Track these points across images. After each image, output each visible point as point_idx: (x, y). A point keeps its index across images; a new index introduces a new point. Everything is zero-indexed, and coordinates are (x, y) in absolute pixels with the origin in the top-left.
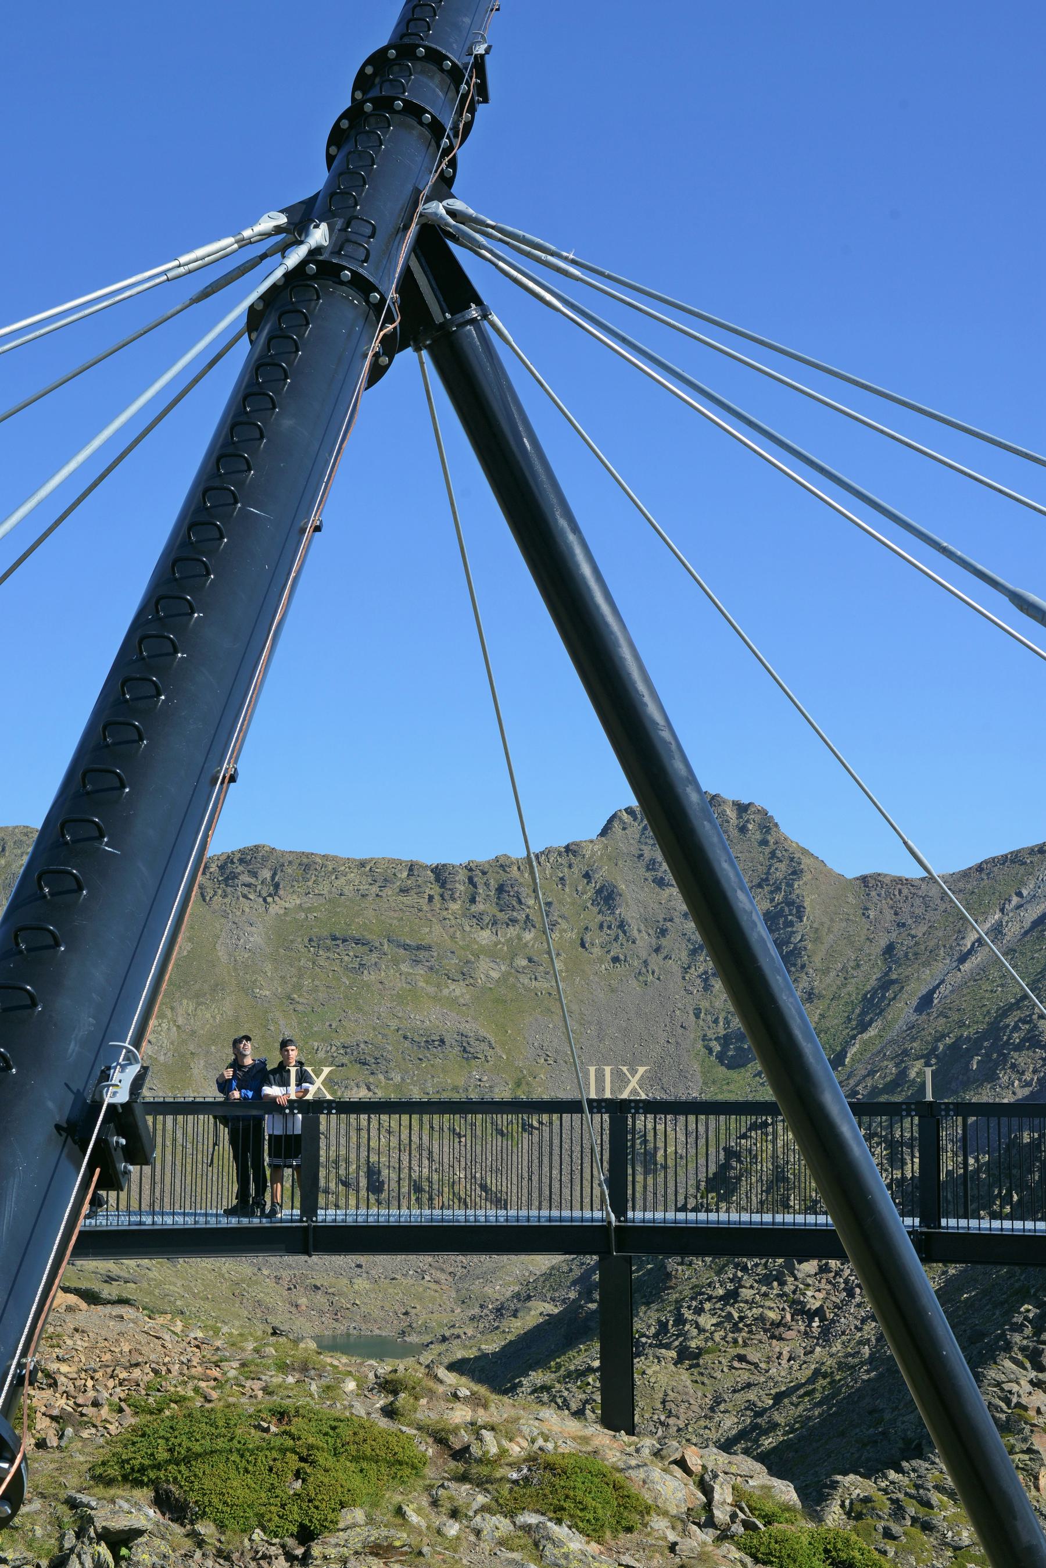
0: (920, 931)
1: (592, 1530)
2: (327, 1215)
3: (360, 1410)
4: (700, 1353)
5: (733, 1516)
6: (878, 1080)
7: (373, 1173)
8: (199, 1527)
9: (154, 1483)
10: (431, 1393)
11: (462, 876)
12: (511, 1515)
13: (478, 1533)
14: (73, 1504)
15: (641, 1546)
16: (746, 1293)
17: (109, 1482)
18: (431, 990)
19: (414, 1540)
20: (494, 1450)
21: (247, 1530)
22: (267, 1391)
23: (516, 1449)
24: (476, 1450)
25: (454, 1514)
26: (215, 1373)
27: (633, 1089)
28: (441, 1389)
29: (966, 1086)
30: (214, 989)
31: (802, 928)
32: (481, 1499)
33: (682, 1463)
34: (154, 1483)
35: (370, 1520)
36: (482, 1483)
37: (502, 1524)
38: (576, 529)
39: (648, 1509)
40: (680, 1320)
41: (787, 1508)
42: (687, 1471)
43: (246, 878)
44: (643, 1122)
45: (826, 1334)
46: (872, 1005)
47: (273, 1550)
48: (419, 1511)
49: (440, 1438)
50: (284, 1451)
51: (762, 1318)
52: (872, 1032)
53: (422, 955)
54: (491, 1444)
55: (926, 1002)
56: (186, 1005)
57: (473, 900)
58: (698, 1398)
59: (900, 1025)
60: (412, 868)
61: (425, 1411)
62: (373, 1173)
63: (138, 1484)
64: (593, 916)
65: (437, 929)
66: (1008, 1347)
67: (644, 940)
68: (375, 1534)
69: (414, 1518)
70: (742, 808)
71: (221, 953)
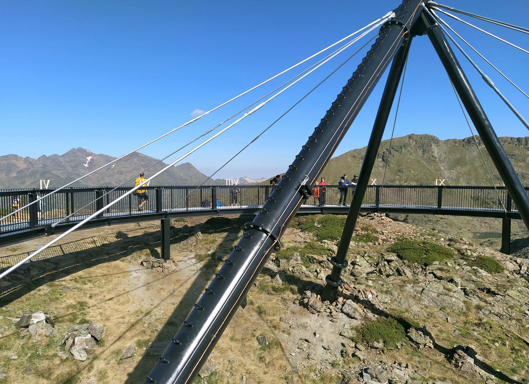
1: (490, 271)
2: (443, 207)
3: (443, 244)
5: (525, 273)
7: (499, 201)
10: (460, 242)
12: (471, 266)
13: (463, 269)
14: (382, 254)
15: (501, 276)
17: (389, 251)
18: (515, 164)
19: (448, 269)
20: (470, 254)
21: (414, 263)
22: (424, 239)
23: (475, 255)
24: (466, 254)
25: (459, 265)
26: (415, 235)
27: (442, 183)
28: (462, 242)
32: (465, 263)
33: (516, 261)
34: (397, 252)
35: (440, 264)
36: (466, 260)
37: (469, 268)
38: (460, 68)
43: (473, 142)
48: (451, 264)
49: (459, 251)
50: (423, 250)
53: (513, 157)
54: (469, 253)
57: (526, 145)
60: (512, 138)
61: (457, 245)
62: (499, 201)
63: (394, 252)
65: (517, 151)
68: (440, 266)
69: (449, 265)
71: (467, 157)
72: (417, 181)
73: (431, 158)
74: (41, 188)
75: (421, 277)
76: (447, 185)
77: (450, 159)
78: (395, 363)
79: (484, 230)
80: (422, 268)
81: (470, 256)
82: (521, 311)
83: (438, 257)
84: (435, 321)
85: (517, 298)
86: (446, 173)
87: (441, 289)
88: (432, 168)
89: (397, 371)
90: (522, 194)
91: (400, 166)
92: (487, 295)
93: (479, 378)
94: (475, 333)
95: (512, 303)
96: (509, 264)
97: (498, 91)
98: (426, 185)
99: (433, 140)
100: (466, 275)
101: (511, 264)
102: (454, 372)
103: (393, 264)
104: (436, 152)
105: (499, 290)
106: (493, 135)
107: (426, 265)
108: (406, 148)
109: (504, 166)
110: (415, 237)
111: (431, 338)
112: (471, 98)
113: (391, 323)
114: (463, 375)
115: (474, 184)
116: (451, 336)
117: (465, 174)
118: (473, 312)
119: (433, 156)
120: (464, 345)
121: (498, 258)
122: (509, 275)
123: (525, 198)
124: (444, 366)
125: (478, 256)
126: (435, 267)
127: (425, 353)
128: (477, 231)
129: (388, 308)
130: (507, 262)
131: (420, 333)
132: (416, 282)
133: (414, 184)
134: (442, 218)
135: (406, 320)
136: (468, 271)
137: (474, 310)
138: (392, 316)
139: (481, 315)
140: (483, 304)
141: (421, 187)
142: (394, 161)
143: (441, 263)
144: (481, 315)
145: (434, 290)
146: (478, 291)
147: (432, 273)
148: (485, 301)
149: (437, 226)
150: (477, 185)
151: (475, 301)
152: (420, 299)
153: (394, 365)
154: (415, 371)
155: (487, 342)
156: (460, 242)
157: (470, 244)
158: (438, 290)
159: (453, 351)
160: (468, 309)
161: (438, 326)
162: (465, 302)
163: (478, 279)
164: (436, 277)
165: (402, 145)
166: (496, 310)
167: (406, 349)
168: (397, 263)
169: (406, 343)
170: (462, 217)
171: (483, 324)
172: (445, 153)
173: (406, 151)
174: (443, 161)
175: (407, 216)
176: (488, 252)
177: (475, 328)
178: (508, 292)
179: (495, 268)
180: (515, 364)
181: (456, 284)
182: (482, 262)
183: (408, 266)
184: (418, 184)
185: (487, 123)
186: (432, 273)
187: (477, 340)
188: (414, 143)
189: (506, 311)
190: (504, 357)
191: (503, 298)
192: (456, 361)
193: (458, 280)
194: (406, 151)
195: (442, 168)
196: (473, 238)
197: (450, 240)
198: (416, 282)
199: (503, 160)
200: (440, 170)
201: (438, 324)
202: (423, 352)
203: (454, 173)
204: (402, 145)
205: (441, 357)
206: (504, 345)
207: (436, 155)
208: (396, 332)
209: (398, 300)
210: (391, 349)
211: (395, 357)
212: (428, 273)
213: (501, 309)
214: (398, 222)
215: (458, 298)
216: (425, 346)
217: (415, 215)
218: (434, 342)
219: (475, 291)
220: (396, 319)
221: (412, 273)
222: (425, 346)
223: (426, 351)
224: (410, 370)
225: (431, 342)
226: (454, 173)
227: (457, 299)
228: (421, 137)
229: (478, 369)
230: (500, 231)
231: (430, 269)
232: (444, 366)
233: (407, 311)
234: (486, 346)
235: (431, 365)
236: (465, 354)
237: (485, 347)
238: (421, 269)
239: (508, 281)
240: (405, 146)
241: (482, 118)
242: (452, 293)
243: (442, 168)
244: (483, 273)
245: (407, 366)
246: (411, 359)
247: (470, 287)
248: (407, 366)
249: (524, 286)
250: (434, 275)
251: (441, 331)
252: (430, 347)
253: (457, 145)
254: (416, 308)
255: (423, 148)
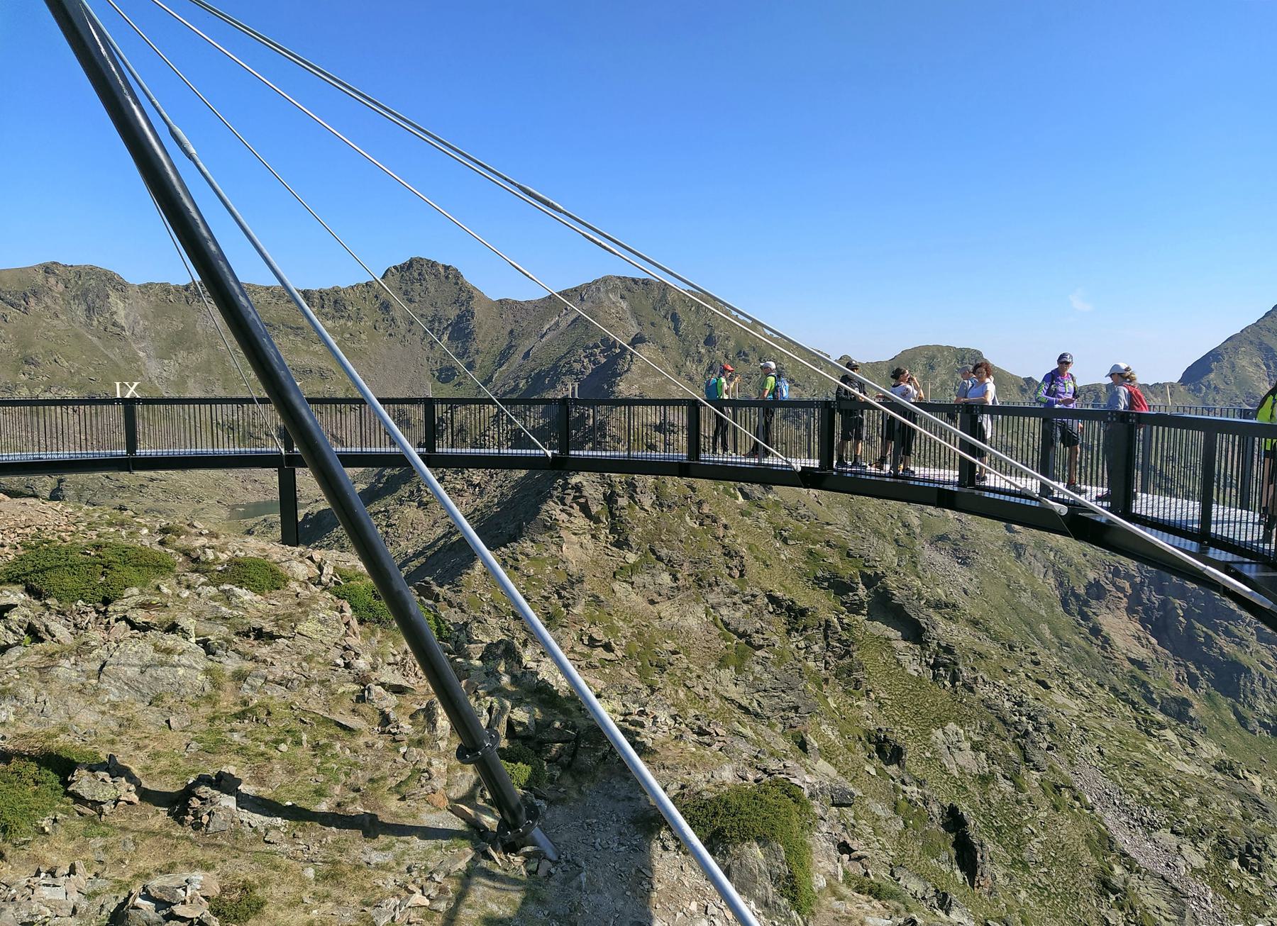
0: (524, 324)
1: (258, 590)
2: (142, 451)
4: (427, 503)
6: (507, 388)
8: (48, 601)
9: (25, 582)
10: (187, 533)
11: (317, 295)
12: (217, 586)
13: (199, 595)
15: (282, 595)
16: (447, 478)
18: (305, 348)
19: (164, 600)
22: (98, 536)
23: (223, 557)
25: (188, 587)
26: (72, 528)
28: (194, 531)
29: (543, 390)
30: (196, 346)
31: (474, 322)
33: (311, 558)
34: (25, 582)
35: (142, 593)
36: (204, 573)
37: (213, 590)
39: (288, 579)
40: (419, 490)
41: (361, 574)
42: (313, 561)
44: (139, 408)
45: (481, 493)
46: (504, 356)
47: (88, 609)
48: (169, 587)
49: (186, 553)
50: (94, 564)
51: (454, 488)
52: (504, 368)
54: (210, 555)
55: (527, 355)
56: (183, 354)
58: (427, 522)
59: (516, 365)
61: (182, 541)
63: (16, 583)
64: (379, 315)
66: (551, 497)
67: (403, 326)
68: (142, 599)
69: (165, 590)
70: (446, 268)
72: (78, 387)
73: (110, 327)
74: (118, 396)
75: (96, 635)
76: (147, 395)
77: (157, 333)
78: (38, 873)
79: (253, 499)
80: (98, 612)
81: (213, 562)
82: (327, 663)
83: (135, 576)
84: (138, 736)
85: (319, 637)
86: (153, 368)
87: (150, 654)
88: (115, 354)
89: (46, 893)
90: (304, 412)
91: (25, 347)
92: (255, 643)
93: (249, 835)
94: (236, 737)
95: (309, 648)
96: (297, 564)
97: (205, 170)
98: (103, 396)
99: (111, 281)
100: (206, 608)
101: (302, 567)
102: (192, 842)
103: (14, 616)
104: (122, 313)
105: (282, 627)
106: (231, 279)
107: (106, 602)
108: (39, 300)
109: (261, 349)
110: (73, 533)
111: (131, 778)
112: (171, 182)
113: (19, 774)
114: (213, 841)
115: (220, 393)
116: (180, 761)
117: (197, 369)
118: (229, 689)
119: (114, 324)
120: (211, 771)
121: (275, 557)
122: (299, 590)
123: (309, 421)
124: (168, 835)
125: (230, 560)
126: (131, 602)
127: (119, 821)
128: (238, 502)
129: (8, 736)
130: (294, 563)
131: (102, 774)
132: (83, 649)
133: (72, 394)
134: (152, 480)
135: (63, 754)
136: (211, 598)
137: (229, 686)
138: (20, 755)
139: (246, 691)
140: (248, 666)
141: (91, 401)
142: (7, 334)
143: (146, 590)
144: (246, 691)
145: (131, 661)
146: (236, 639)
147: (125, 618)
148: (254, 659)
149: (143, 500)
150: (229, 396)
151: (231, 664)
152: (97, 691)
153: (37, 879)
154: (96, 875)
155: (263, 748)
156: (187, 533)
157: (212, 535)
158: (141, 659)
159: (189, 792)
160: (216, 685)
161: (146, 747)
162: (207, 671)
163: (235, 613)
164: (133, 625)
165: (28, 290)
166: (278, 671)
167: (67, 828)
168: (26, 611)
169: (66, 812)
170: (201, 472)
171: (251, 710)
172: (145, 317)
173: (41, 306)
174: (143, 338)
175: (60, 481)
176: (253, 547)
177: (236, 724)
178: (300, 627)
179: (266, 578)
180: (321, 778)
181: (185, 634)
182: (240, 572)
183: (58, 612)
184: (84, 395)
185: (213, 248)
186: (125, 618)
187: (241, 751)
188: (61, 287)
189: (298, 670)
190: (299, 770)
191: (290, 643)
192: (196, 814)
193: (187, 623)
194: (41, 306)
195: (141, 354)
196: (230, 519)
197: (164, 531)
198: (83, 649)
199: (258, 337)
200: (136, 359)
201: (147, 741)
202: (111, 820)
203: (171, 368)
204: (28, 290)
205: (159, 818)
206: (298, 743)
207: (121, 318)
208: (36, 794)
209: (38, 707)
210: (25, 843)
211: (37, 859)
212: (112, 621)
213: (288, 668)
214: (22, 500)
215: (190, 667)
216: (115, 804)
217: (82, 477)
218: (138, 786)
219: (228, 641)
220: (32, 758)
221: (72, 629)
222: (115, 804)
223: (120, 815)
224: (82, 878)
225: (133, 788)
226: (171, 368)
227: (190, 669)
228: (79, 272)
229: (246, 815)
230: (276, 496)
231: (119, 608)
232: (168, 835)
233: (64, 730)
234: (261, 758)
235: (136, 844)
236: (216, 792)
237: (260, 761)
238: (94, 615)
239: (299, 604)
240: (35, 294)
241: (201, 234)
242: (176, 657)
243: (141, 354)
244: (245, 595)
245: (72, 870)
246: (82, 848)
247: (217, 633)
248: (72, 870)
249: (331, 608)
250: (129, 622)
251: (155, 756)
252: (130, 803)
253: (171, 297)
254: (87, 717)
255: (85, 300)
